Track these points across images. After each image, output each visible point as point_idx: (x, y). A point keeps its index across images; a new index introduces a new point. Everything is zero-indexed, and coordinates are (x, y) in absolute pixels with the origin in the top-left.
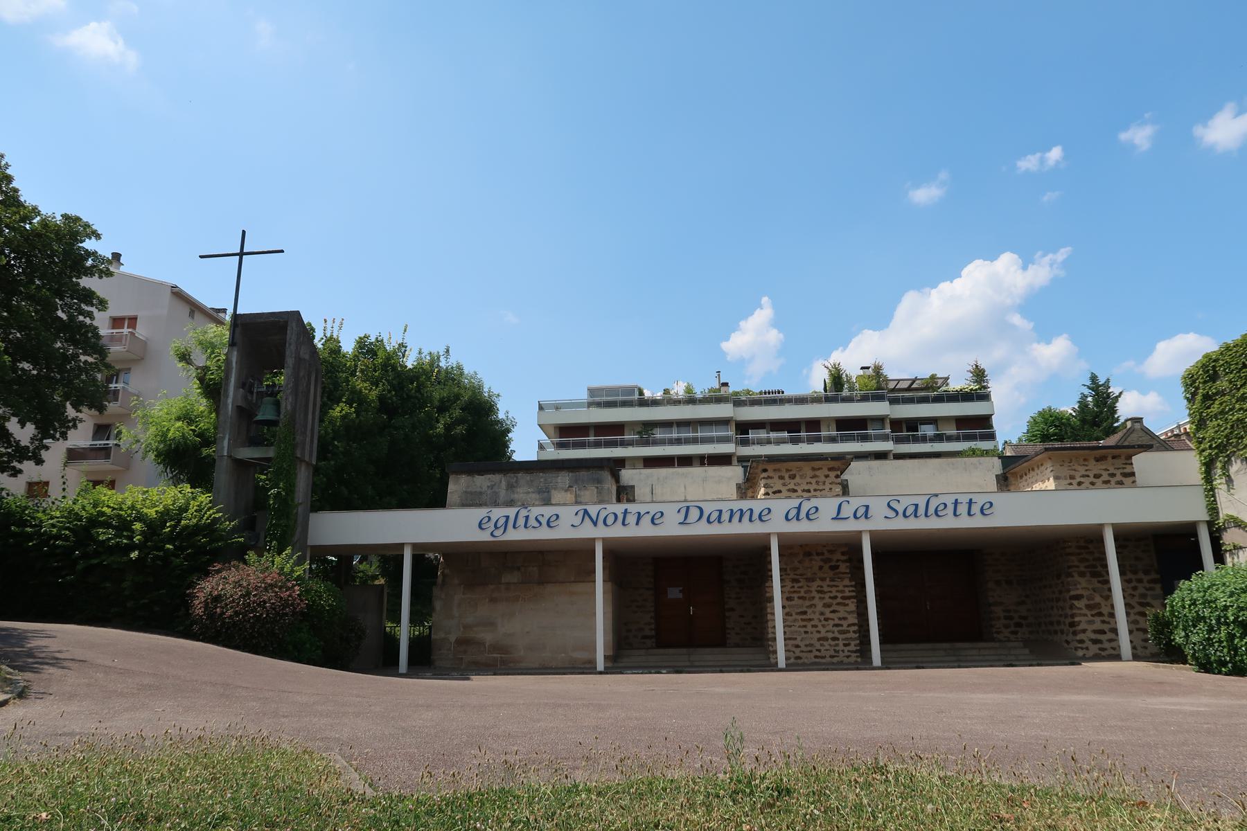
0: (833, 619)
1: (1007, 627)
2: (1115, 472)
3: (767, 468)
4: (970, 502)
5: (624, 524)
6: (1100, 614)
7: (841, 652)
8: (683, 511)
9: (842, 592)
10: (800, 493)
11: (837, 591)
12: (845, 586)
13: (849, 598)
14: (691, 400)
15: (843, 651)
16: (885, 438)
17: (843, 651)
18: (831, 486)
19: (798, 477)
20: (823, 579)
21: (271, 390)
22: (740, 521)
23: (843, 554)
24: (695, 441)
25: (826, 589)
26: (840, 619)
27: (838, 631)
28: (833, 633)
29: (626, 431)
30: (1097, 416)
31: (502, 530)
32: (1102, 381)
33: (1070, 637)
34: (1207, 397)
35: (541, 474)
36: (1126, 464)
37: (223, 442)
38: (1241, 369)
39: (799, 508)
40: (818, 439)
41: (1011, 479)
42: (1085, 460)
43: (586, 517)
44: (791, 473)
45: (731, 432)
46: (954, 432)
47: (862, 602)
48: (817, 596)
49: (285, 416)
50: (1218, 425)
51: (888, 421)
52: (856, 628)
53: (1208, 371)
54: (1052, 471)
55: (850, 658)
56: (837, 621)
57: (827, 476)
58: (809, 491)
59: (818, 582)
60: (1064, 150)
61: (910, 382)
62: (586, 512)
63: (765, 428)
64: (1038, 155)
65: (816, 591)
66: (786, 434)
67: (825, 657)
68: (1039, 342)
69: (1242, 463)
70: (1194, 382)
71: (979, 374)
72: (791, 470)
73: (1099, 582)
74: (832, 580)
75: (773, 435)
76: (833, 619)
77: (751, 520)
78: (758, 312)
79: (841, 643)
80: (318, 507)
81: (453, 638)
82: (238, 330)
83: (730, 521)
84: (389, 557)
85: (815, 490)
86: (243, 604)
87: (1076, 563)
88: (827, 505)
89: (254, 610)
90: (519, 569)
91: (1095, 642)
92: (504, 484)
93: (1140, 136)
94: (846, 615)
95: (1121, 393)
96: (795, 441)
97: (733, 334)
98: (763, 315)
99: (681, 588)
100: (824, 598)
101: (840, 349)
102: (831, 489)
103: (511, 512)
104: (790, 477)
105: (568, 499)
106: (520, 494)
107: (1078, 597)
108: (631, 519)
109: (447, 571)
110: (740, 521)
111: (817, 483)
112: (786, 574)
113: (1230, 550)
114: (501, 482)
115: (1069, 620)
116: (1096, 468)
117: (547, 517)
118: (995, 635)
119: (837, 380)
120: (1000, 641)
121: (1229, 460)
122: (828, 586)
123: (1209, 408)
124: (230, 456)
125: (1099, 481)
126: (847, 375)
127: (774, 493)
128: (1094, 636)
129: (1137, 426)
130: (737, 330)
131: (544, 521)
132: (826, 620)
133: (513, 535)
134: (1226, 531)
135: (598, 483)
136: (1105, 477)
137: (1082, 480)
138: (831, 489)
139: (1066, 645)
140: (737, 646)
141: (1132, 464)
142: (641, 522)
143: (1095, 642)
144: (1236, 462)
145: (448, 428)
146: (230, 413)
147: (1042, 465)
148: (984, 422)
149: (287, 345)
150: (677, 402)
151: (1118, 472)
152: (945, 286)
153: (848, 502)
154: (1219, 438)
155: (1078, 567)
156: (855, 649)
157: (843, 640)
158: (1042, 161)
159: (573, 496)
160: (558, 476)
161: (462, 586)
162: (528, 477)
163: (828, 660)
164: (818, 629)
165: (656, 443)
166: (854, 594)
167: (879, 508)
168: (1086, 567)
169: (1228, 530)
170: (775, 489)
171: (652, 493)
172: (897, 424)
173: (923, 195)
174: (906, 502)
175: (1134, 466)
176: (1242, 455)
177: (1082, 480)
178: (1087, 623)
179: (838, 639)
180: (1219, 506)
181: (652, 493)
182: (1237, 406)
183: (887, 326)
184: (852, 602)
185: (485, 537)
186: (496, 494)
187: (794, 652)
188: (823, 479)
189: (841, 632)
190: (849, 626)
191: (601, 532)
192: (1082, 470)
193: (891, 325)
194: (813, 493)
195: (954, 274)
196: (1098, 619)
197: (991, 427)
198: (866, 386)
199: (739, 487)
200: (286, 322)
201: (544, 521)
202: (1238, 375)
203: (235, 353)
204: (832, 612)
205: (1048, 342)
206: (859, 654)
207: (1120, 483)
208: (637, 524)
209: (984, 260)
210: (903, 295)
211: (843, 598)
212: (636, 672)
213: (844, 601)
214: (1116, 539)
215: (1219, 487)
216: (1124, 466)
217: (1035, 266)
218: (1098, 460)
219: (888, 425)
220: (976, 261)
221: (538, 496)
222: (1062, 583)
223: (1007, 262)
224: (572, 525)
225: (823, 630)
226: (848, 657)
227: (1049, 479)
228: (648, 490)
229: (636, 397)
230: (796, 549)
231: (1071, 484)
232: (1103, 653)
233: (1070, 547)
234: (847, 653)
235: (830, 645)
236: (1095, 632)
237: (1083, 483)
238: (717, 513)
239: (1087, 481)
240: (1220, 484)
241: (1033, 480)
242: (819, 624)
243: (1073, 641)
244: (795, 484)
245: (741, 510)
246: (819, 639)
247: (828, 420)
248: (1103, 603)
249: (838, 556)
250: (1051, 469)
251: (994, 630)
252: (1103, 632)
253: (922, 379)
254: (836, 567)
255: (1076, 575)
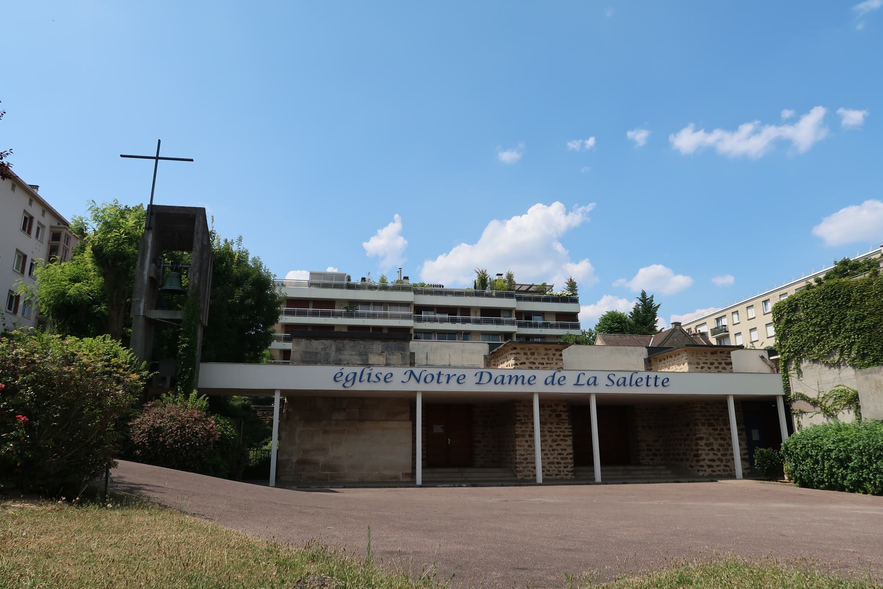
0: (558, 450)
1: (648, 455)
2: (721, 362)
3: (517, 347)
4: (656, 378)
5: (438, 382)
6: (712, 449)
7: (562, 472)
8: (479, 375)
9: (563, 432)
10: (537, 365)
11: (561, 431)
12: (565, 428)
13: (568, 436)
14: (384, 288)
15: (563, 471)
16: (512, 323)
17: (563, 471)
18: (557, 361)
19: (536, 354)
20: (552, 423)
21: (175, 266)
22: (516, 383)
23: (564, 406)
24: (385, 316)
25: (554, 430)
26: (562, 450)
27: (561, 458)
28: (558, 459)
29: (336, 306)
30: (645, 319)
31: (351, 382)
32: (648, 296)
33: (694, 464)
34: (788, 321)
35: (361, 342)
36: (727, 357)
37: (139, 304)
38: (815, 307)
39: (553, 377)
40: (468, 321)
41: (653, 362)
42: (705, 353)
43: (412, 376)
44: (532, 351)
45: (410, 312)
46: (554, 322)
47: (414, 426)
48: (548, 434)
49: (193, 288)
50: (796, 339)
51: (514, 312)
52: (571, 456)
53: (792, 306)
54: (687, 359)
55: (568, 476)
56: (560, 452)
57: (554, 355)
58: (543, 364)
59: (549, 425)
60: (596, 140)
61: (529, 286)
62: (412, 372)
63: (433, 311)
64: (581, 141)
65: (548, 431)
66: (447, 316)
67: (552, 475)
68: (571, 263)
69: (810, 362)
70: (781, 311)
71: (572, 285)
72: (531, 349)
73: (712, 429)
74: (557, 424)
75: (438, 316)
76: (558, 450)
77: (523, 383)
78: (391, 224)
79: (562, 466)
80: (206, 359)
81: (294, 459)
82: (153, 218)
83: (509, 383)
84: (263, 398)
85: (547, 364)
86: (181, 434)
87: (700, 418)
88: (542, 375)
89: (189, 440)
90: (344, 410)
91: (710, 466)
92: (334, 348)
93: (640, 136)
94: (566, 447)
95: (659, 305)
96: (454, 321)
97: (372, 238)
98: (394, 227)
99: (442, 426)
100: (552, 436)
101: (445, 254)
102: (557, 363)
103: (358, 370)
104: (531, 354)
105: (380, 361)
106: (346, 355)
107: (701, 439)
108: (443, 379)
109: (290, 410)
110: (516, 383)
111: (548, 359)
112: (528, 419)
113: (797, 414)
114: (332, 345)
115: (695, 453)
116: (711, 358)
117: (384, 375)
118: (641, 461)
119: (483, 281)
120: (644, 465)
121: (801, 359)
122: (555, 428)
123: (789, 328)
124: (144, 316)
125: (713, 367)
126: (490, 279)
127: (521, 364)
128: (709, 463)
129: (678, 327)
130: (375, 235)
131: (382, 378)
132: (553, 450)
133: (359, 387)
134: (795, 402)
135: (402, 351)
136: (716, 364)
137: (703, 365)
138: (557, 363)
139: (690, 468)
140: (482, 466)
141: (731, 357)
142: (450, 381)
143: (710, 466)
144: (805, 362)
145: (242, 299)
146: (146, 282)
147: (679, 354)
148: (573, 316)
149: (195, 233)
150: (372, 288)
151: (723, 362)
152: (516, 219)
153: (584, 374)
154: (796, 347)
155: (701, 420)
156: (570, 469)
157: (564, 464)
158: (583, 145)
159: (385, 359)
160: (374, 344)
161: (303, 421)
162: (352, 344)
163: (554, 477)
164: (548, 456)
165: (359, 316)
166: (571, 433)
167: (602, 379)
168: (705, 420)
169: (796, 401)
170: (521, 362)
171: (427, 359)
172: (520, 314)
173: (508, 156)
174: (619, 375)
175: (732, 358)
176: (810, 358)
177: (703, 365)
178: (705, 455)
179: (560, 463)
180: (791, 387)
181: (427, 359)
182: (811, 329)
183: (476, 242)
184: (570, 439)
185: (338, 387)
186: (328, 355)
187: (532, 472)
188: (551, 356)
189: (562, 459)
190: (568, 454)
191: (422, 387)
192: (703, 359)
193: (479, 242)
194: (545, 365)
195: (522, 211)
196: (711, 452)
197: (578, 320)
198: (503, 288)
199: (485, 357)
200: (195, 216)
201: (382, 378)
202: (813, 310)
203: (151, 235)
204: (557, 445)
205: (577, 263)
206: (573, 473)
207: (724, 368)
208: (448, 382)
209: (543, 204)
210: (489, 222)
211: (564, 436)
212: (445, 485)
213: (565, 438)
214: (735, 404)
215: (793, 375)
216: (726, 358)
217: (573, 213)
218: (712, 353)
219: (514, 314)
220: (538, 204)
221: (359, 358)
222: (691, 430)
223: (557, 207)
224: (402, 382)
225: (551, 457)
226: (567, 475)
227: (684, 364)
228: (424, 356)
229: (346, 282)
230: (547, 402)
231: (697, 368)
232: (714, 474)
233: (697, 407)
234: (566, 473)
235: (555, 467)
236: (710, 460)
237: (704, 367)
238: (501, 378)
239: (706, 366)
240: (793, 374)
241: (671, 363)
242: (549, 453)
243: (696, 465)
244: (534, 359)
245: (517, 376)
246: (549, 463)
247: (476, 308)
248: (714, 442)
249: (561, 408)
250: (686, 357)
251: (641, 458)
252: (713, 460)
253: (536, 285)
254: (558, 416)
255: (700, 424)
